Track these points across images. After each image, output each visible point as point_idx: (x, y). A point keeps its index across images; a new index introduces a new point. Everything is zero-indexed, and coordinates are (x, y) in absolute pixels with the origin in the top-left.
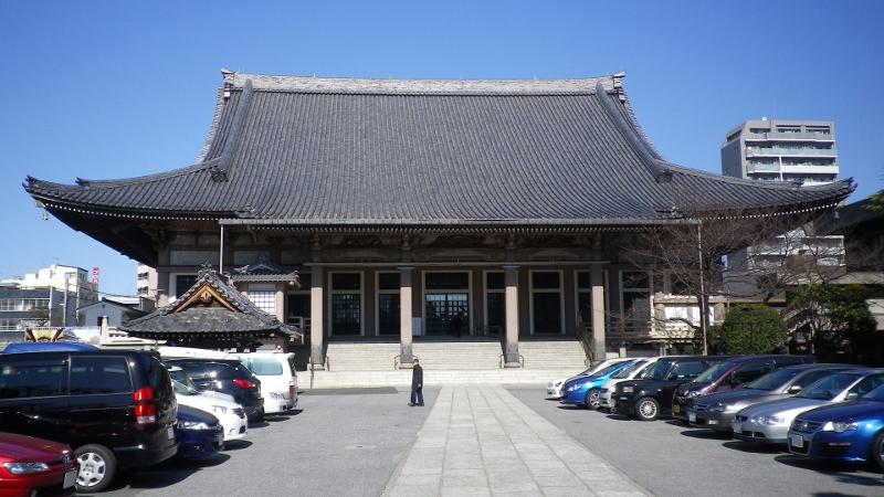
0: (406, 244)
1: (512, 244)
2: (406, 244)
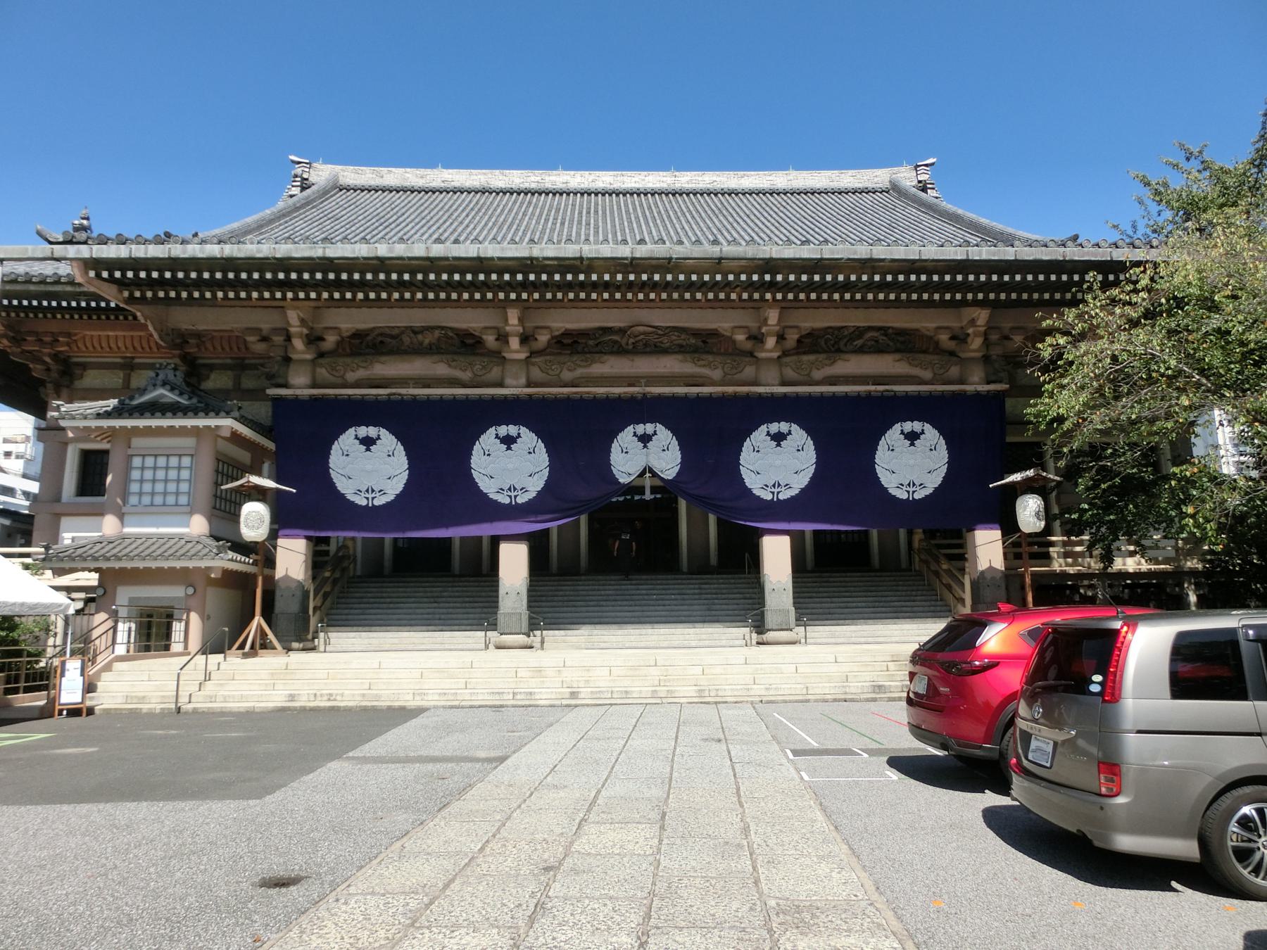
0: (514, 343)
1: (771, 342)
2: (514, 343)
